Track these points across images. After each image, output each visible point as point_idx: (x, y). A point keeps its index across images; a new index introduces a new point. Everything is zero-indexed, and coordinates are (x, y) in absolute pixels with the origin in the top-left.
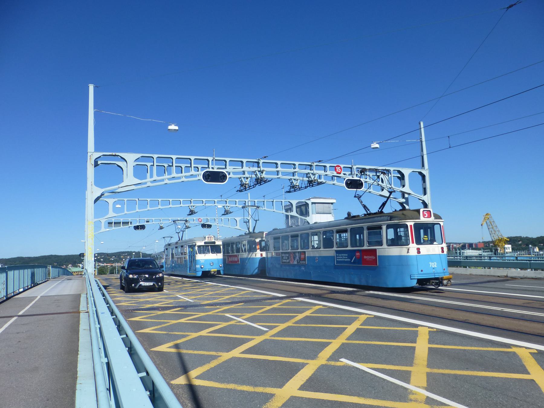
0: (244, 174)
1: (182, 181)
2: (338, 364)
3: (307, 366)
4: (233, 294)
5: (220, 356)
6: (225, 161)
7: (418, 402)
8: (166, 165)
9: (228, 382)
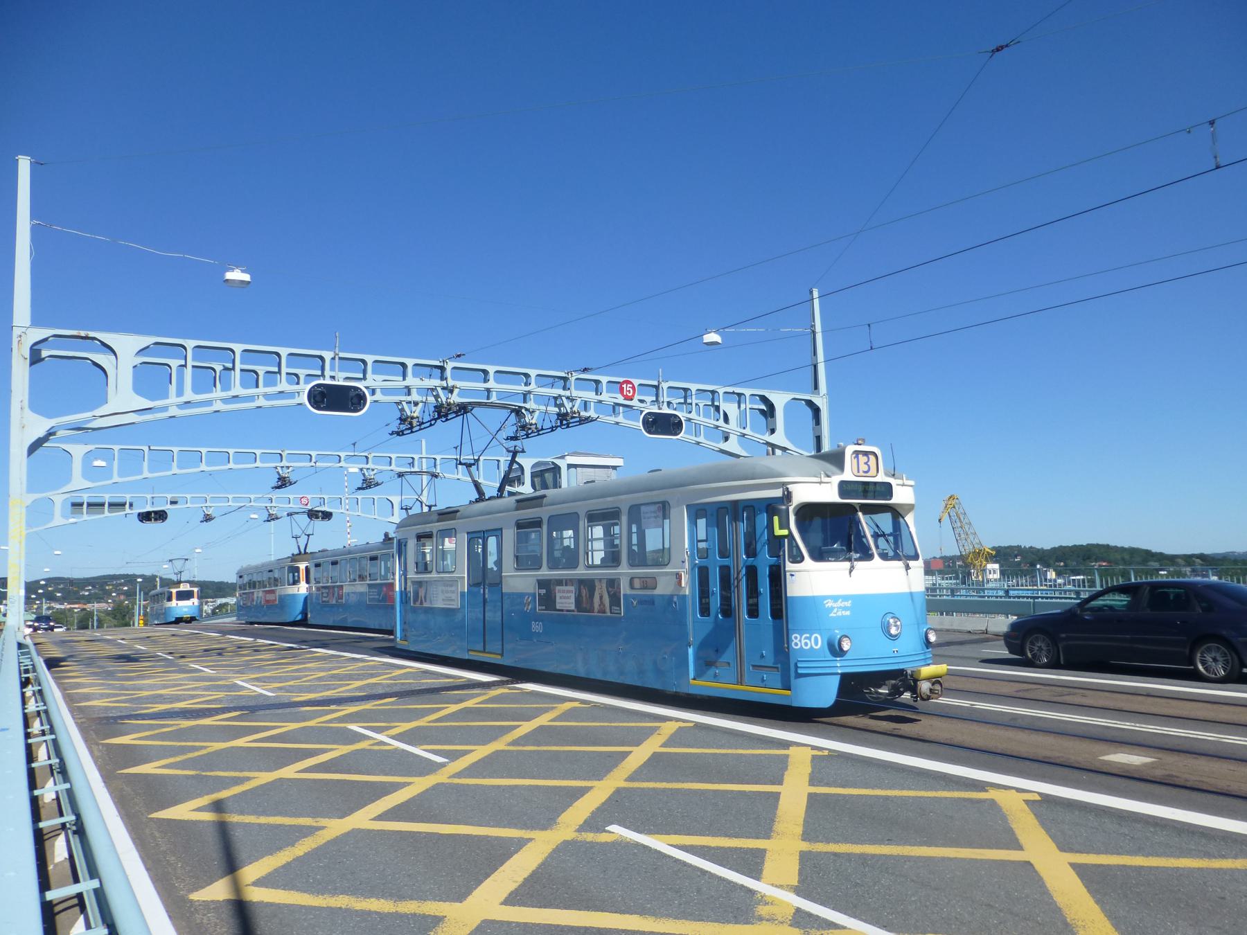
0: (409, 393)
1: (258, 407)
2: (603, 838)
3: (529, 845)
4: (372, 676)
5: (323, 828)
6: (364, 362)
7: (776, 922)
8: (219, 368)
9: (335, 892)
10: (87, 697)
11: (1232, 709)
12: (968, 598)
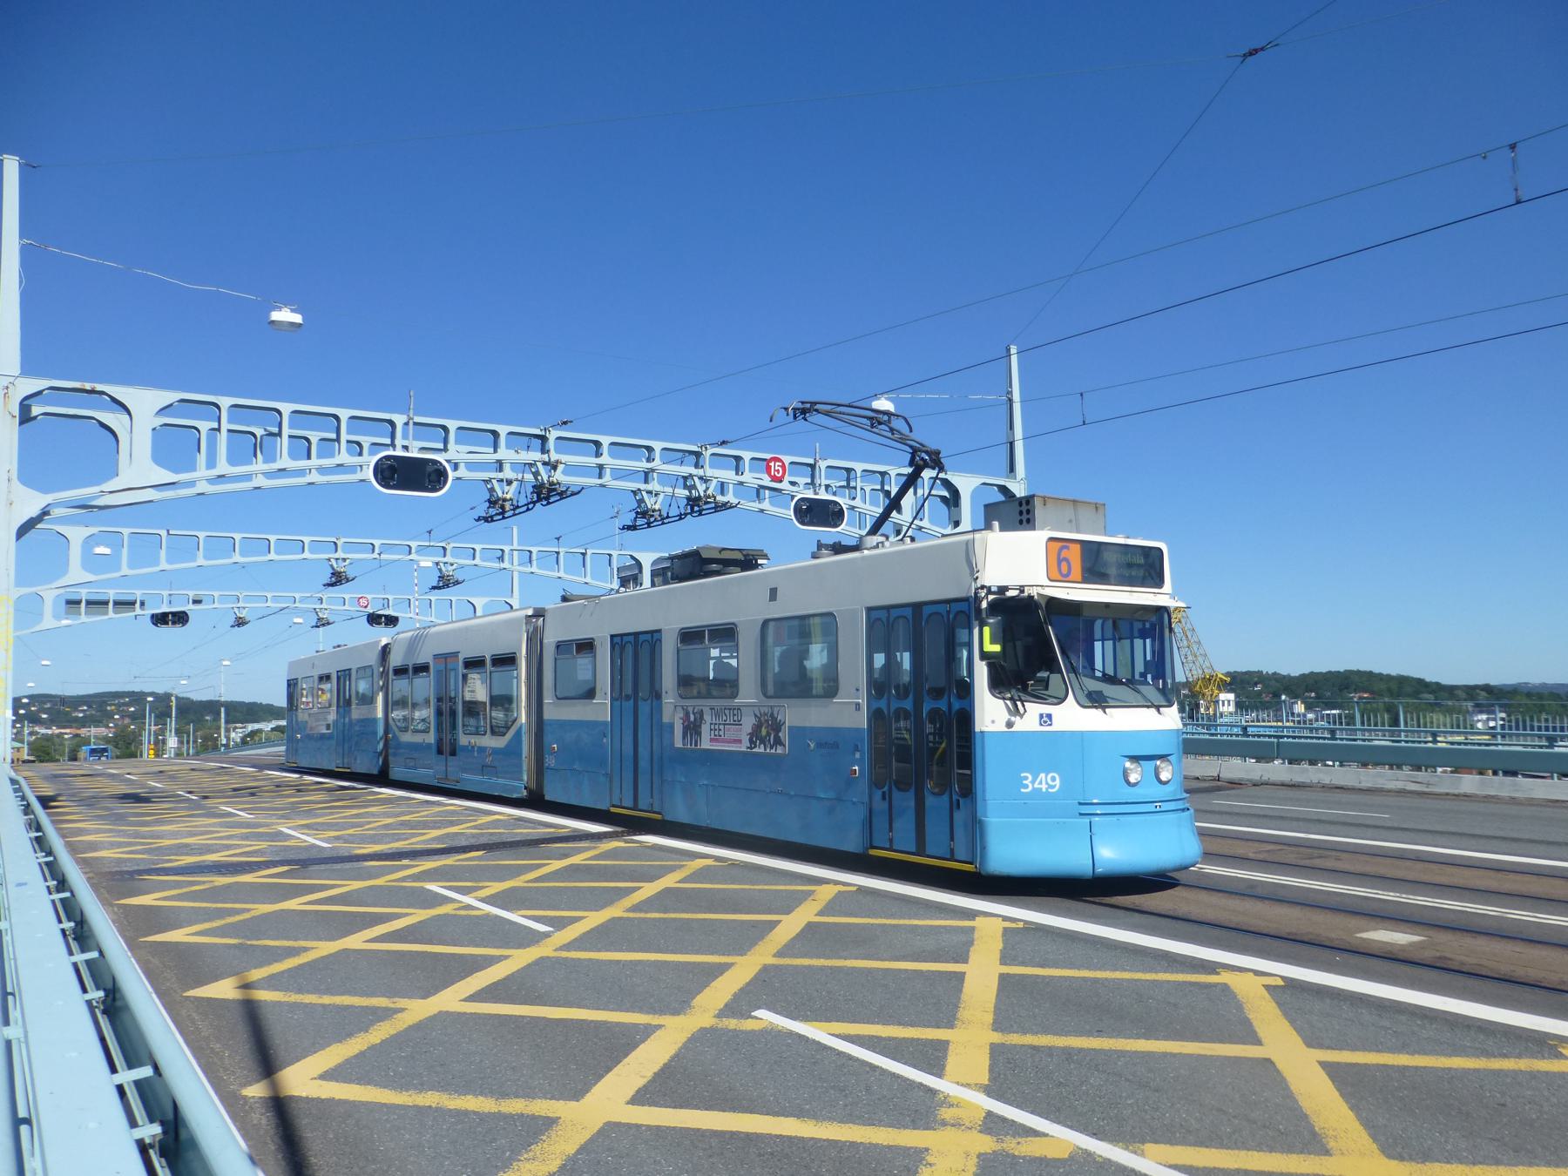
0: (501, 469)
2: (748, 1025)
3: (658, 1033)
4: (452, 824)
5: (402, 1010)
6: (445, 428)
7: (963, 1127)
9: (422, 1087)
10: (94, 846)
11: (1519, 877)
12: (1196, 736)
